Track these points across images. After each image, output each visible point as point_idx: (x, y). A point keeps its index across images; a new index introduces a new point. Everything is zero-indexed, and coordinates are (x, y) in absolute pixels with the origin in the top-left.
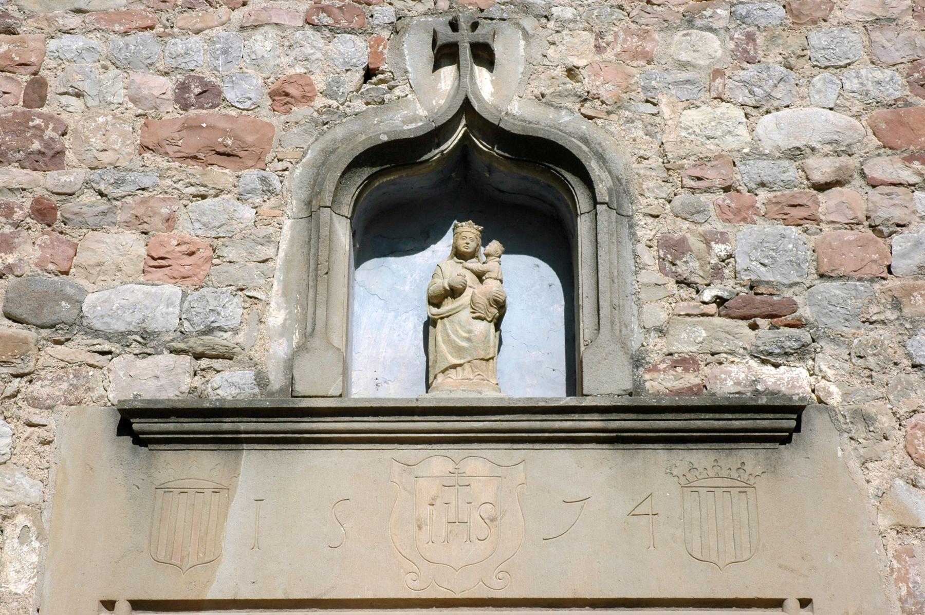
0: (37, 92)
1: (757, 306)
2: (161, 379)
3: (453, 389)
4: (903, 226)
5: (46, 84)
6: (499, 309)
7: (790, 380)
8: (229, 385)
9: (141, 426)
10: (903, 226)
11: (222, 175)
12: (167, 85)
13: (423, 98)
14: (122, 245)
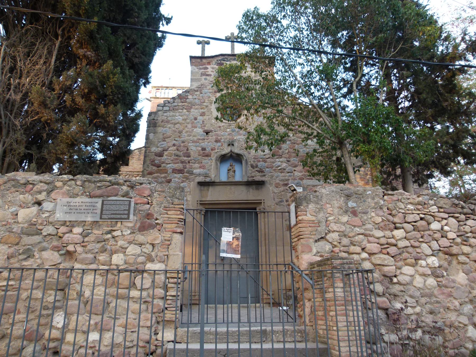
0: (187, 150)
1: (261, 171)
2: (201, 179)
3: (231, 180)
4: (148, 99)
5: (387, 183)
6: (234, 171)
7: (263, 179)
8: (208, 180)
9: (201, 184)
10: (148, 99)
11: (206, 158)
12: (200, 149)
13: (226, 150)
14: (197, 165)
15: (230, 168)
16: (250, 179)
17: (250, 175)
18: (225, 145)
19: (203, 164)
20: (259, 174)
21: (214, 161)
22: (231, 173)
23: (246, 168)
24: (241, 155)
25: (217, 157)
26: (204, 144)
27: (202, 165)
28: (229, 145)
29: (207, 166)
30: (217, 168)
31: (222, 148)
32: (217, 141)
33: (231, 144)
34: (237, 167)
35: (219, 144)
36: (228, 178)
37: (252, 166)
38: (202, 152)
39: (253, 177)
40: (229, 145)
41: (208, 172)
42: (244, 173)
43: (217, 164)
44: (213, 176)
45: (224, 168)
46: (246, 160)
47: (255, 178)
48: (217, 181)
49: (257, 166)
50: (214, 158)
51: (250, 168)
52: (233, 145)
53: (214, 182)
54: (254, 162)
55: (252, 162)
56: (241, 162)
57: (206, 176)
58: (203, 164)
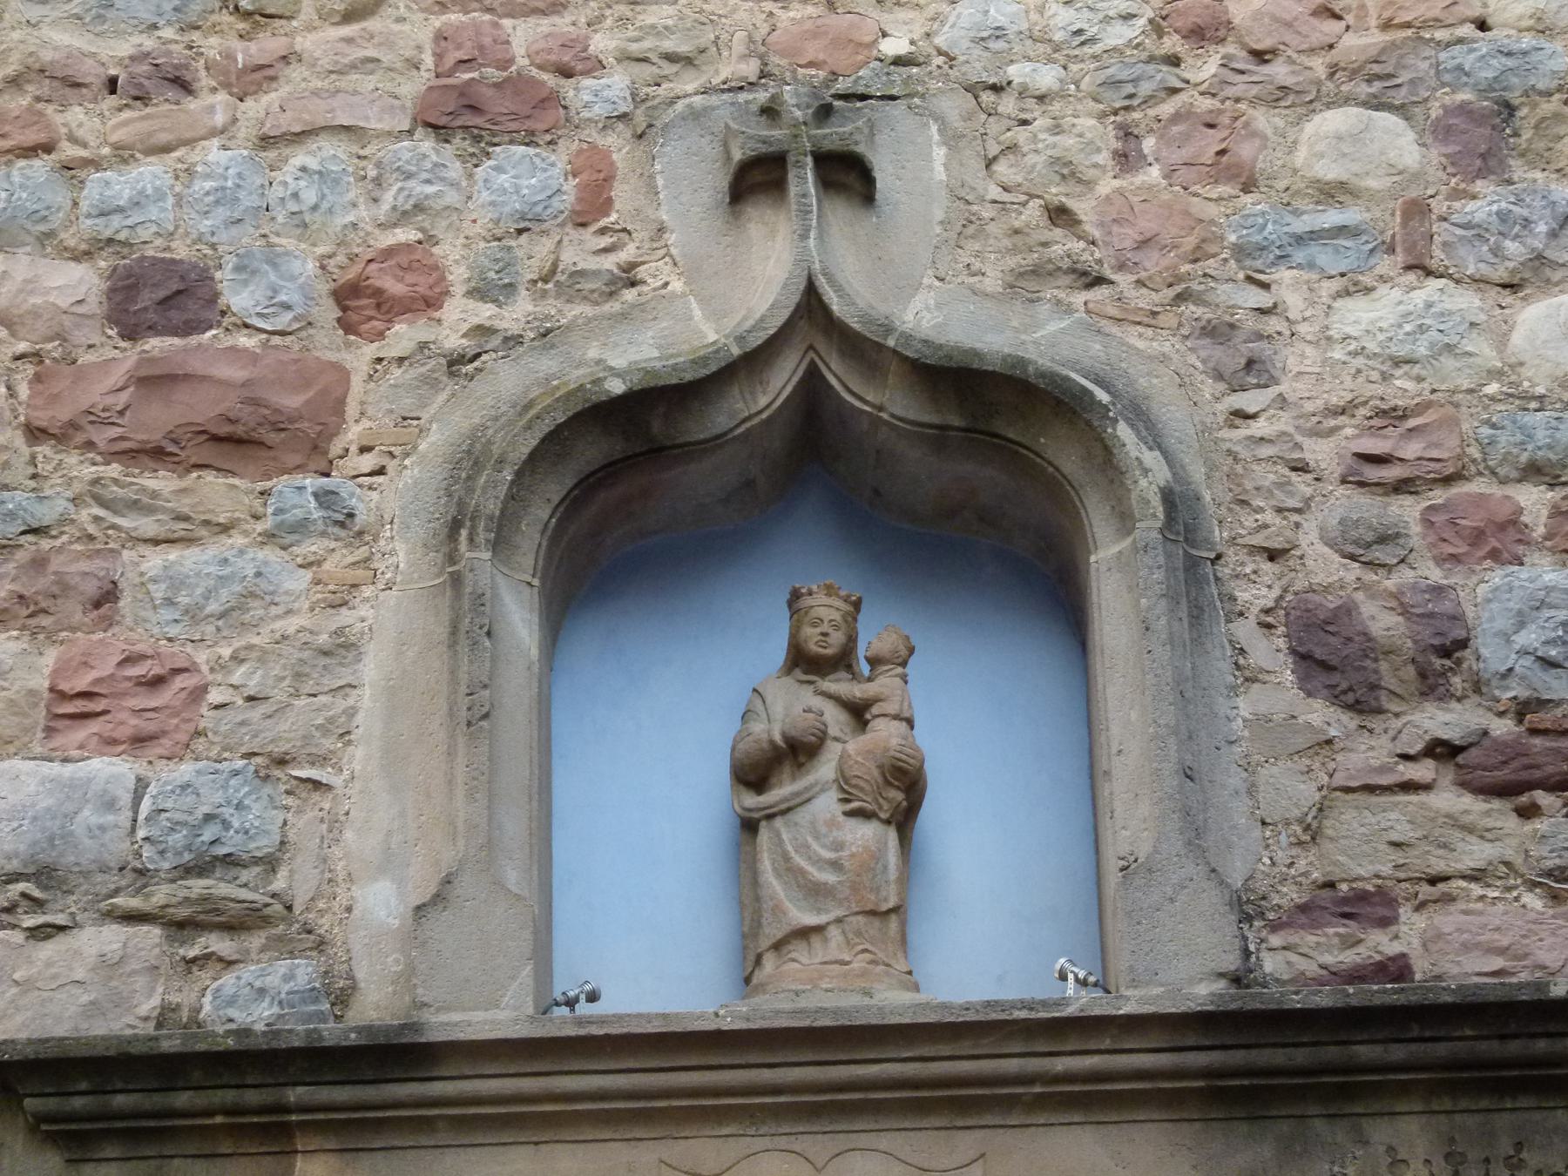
3: (812, 988)
6: (901, 794)
8: (250, 996)
11: (218, 492)
12: (75, 284)
13: (705, 293)
15: (794, 705)
16: (1301, 964)
17: (1290, 874)
18: (678, 187)
19: (145, 626)
20: (1495, 834)
21: (403, 554)
22: (823, 826)
23: (1187, 696)
24: (1404, 955)
25: (470, 460)
26: (153, 197)
27: (101, 654)
28: (756, 179)
29: (228, 672)
30: (476, 716)
31: (581, 252)
32: (466, 113)
33: (806, 158)
34: (961, 700)
35: (521, 175)
36: (757, 945)
37: (1330, 657)
38: (111, 361)
39: (1365, 905)
40: (756, 179)
41: (257, 819)
42: (1135, 824)
43: (467, 623)
44: (380, 903)
45: (659, 726)
46: (1179, 508)
47: (1407, 936)
48: (486, 1005)
49: (1443, 656)
50: (400, 500)
51: (1281, 693)
52: (847, 175)
53: (398, 1055)
54: (1369, 547)
55: (1323, 566)
56: (1055, 593)
57: (211, 902)
58: (145, 626)
